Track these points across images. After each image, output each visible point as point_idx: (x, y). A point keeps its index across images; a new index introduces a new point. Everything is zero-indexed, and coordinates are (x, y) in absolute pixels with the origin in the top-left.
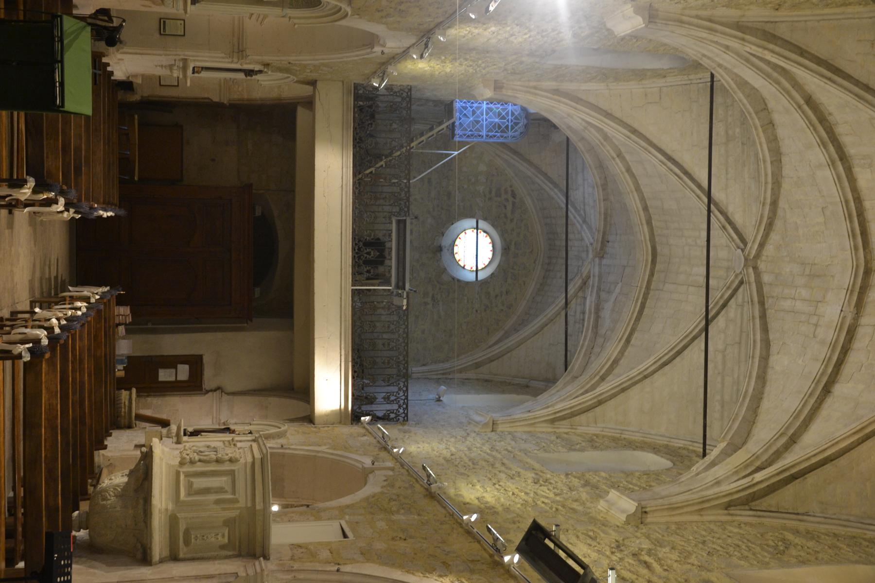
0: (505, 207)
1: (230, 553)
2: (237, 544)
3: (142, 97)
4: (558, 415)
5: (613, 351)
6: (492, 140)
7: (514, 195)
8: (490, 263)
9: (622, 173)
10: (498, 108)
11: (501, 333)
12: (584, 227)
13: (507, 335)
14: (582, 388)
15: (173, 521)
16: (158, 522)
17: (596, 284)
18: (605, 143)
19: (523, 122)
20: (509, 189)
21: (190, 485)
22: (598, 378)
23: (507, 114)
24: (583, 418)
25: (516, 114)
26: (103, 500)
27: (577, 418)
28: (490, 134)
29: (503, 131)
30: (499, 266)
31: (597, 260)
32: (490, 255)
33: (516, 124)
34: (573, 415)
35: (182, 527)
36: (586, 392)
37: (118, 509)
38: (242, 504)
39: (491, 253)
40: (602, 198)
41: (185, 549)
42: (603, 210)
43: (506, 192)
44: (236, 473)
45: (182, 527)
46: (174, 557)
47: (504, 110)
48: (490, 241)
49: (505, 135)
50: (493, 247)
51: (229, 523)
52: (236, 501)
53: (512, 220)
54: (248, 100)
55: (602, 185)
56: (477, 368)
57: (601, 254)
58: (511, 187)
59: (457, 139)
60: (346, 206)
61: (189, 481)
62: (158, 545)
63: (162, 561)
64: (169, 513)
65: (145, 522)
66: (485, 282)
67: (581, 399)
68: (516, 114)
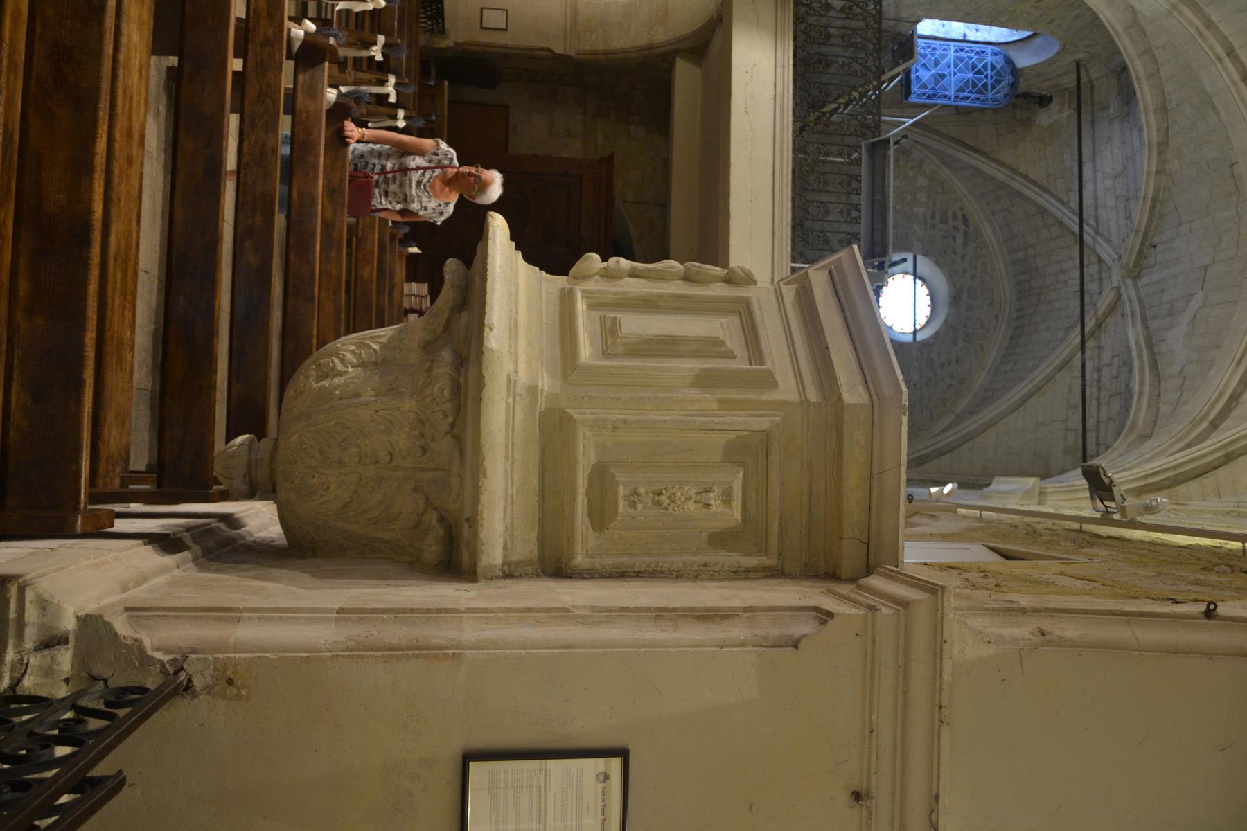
0: (954, 238)
1: (753, 561)
2: (774, 529)
3: (456, 43)
4: (1151, 480)
5: (1229, 381)
6: (963, 104)
7: (966, 222)
8: (932, 311)
9: (1235, 84)
10: (971, 58)
11: (952, 417)
12: (1099, 239)
13: (958, 420)
14: (1180, 440)
15: (554, 431)
16: (502, 422)
17: (1138, 311)
18: (1206, 32)
19: (1008, 79)
20: (959, 213)
21: (609, 331)
22: (1205, 424)
23: (985, 67)
24: (1194, 486)
25: (998, 67)
26: (320, 378)
27: (1182, 489)
28: (962, 95)
29: (979, 92)
30: (946, 321)
31: (1129, 282)
32: (928, 311)
33: (998, 82)
34: (1177, 481)
35: (585, 456)
36: (1188, 446)
37: (368, 396)
38: (787, 390)
39: (929, 309)
40: (1154, 169)
41: (593, 540)
42: (1151, 192)
43: (955, 218)
44: (755, 307)
45: (585, 456)
46: (555, 566)
47: (980, 60)
48: (927, 291)
49: (983, 97)
50: (932, 300)
51: (750, 452)
52: (769, 381)
53: (963, 257)
54: (605, 53)
55: (1159, 144)
56: (919, 465)
57: (1136, 272)
58: (962, 209)
59: (913, 99)
60: (782, 130)
61: (603, 320)
62: (501, 516)
63: (510, 573)
64: (541, 405)
65: (458, 439)
66: (925, 344)
67: (1194, 451)
68: (998, 67)
